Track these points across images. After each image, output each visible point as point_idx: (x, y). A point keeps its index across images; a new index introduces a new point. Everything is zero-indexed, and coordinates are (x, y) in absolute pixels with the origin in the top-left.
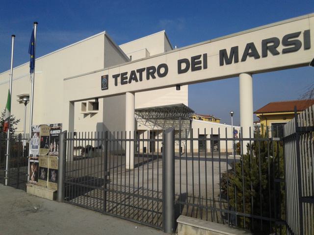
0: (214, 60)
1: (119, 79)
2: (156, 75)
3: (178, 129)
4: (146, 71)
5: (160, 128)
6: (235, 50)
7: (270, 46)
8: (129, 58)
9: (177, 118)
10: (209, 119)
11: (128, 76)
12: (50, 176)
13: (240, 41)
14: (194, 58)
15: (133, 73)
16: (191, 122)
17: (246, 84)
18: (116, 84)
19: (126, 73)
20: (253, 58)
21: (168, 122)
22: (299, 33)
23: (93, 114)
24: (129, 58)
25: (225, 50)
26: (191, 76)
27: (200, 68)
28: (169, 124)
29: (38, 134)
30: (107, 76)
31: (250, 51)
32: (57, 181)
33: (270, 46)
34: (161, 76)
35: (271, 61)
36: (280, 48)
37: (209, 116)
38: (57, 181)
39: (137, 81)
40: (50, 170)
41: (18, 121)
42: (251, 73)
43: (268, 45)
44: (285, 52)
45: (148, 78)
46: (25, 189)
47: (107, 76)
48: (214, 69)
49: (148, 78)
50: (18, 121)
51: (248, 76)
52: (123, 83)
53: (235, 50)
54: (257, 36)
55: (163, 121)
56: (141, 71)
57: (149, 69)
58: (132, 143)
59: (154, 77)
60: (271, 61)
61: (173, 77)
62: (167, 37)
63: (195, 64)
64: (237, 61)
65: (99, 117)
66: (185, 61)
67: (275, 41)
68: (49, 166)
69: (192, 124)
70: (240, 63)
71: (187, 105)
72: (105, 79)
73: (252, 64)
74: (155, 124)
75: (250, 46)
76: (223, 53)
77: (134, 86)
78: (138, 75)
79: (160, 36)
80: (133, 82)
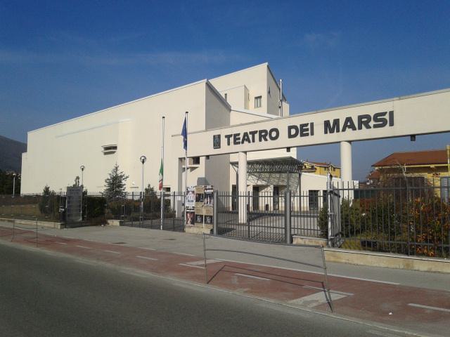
0: (319, 129)
1: (232, 139)
2: (268, 137)
3: (285, 184)
4: (258, 133)
5: (264, 183)
6: (336, 122)
7: (364, 121)
8: (224, 97)
9: (285, 172)
10: (325, 168)
11: (241, 136)
12: (206, 220)
13: (341, 114)
14: (302, 126)
15: (246, 134)
16: (300, 175)
17: (346, 150)
18: (229, 144)
19: (239, 134)
20: (351, 129)
21: (273, 175)
22: (386, 113)
23: (193, 169)
24: (224, 97)
25: (329, 121)
26: (300, 140)
27: (307, 135)
28: (276, 179)
29: (193, 192)
30: (219, 136)
31: (349, 124)
32: (212, 222)
33: (364, 121)
34: (273, 139)
35: (364, 133)
36: (372, 123)
37: (326, 164)
38: (212, 222)
39: (249, 142)
40: (205, 216)
41: (127, 177)
42: (350, 142)
43: (363, 120)
44: (375, 126)
45: (260, 140)
46: (183, 231)
47: (219, 136)
48: (320, 136)
49: (260, 140)
50: (127, 177)
51: (348, 144)
52: (235, 143)
53: (336, 122)
54: (354, 112)
55: (267, 175)
56: (253, 133)
57: (261, 132)
58: (272, 198)
59: (266, 140)
60: (364, 133)
61: (284, 140)
62: (270, 71)
63: (303, 130)
64: (338, 131)
65: (201, 171)
66: (295, 127)
67: (368, 117)
68: (204, 213)
69: (302, 177)
70: (341, 132)
71: (295, 157)
72: (217, 139)
73: (350, 134)
74: (259, 178)
75: (349, 120)
76: (327, 123)
77: (246, 146)
78: (250, 136)
79: (261, 70)
80: (246, 142)
